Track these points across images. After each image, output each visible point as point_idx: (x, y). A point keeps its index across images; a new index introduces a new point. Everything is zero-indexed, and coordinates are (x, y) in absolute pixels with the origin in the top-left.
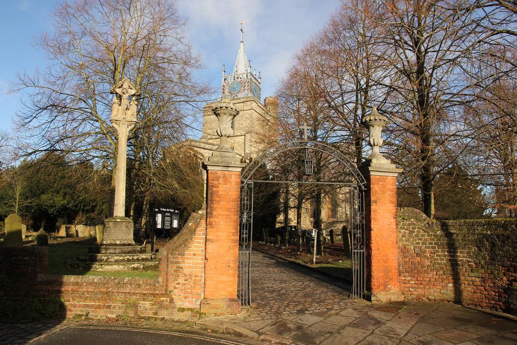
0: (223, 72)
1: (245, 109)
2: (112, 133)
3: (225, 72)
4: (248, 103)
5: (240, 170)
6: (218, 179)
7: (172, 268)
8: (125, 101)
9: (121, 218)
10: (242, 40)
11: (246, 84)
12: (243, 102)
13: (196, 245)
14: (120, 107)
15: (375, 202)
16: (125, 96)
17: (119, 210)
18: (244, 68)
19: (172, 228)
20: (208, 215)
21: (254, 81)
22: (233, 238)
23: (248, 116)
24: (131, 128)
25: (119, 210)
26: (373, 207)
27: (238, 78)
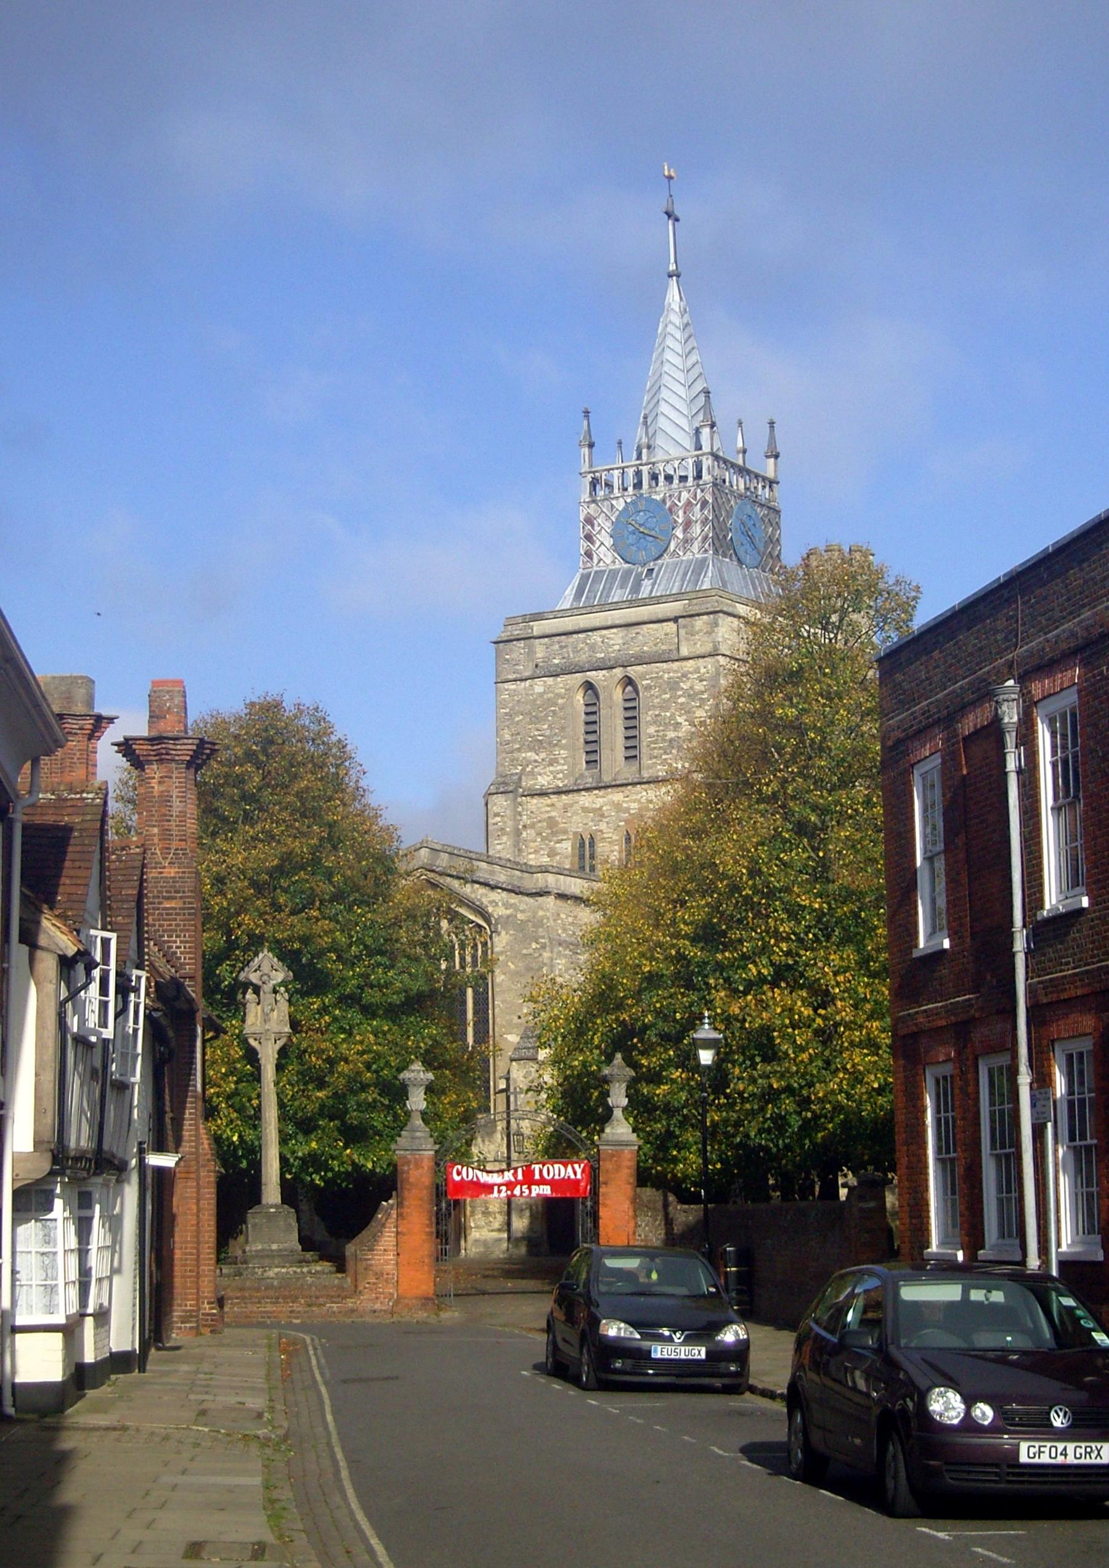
0: (586, 450)
1: (685, 651)
2: (252, 1056)
3: (591, 446)
4: (700, 623)
5: (432, 1153)
6: (408, 1163)
7: (361, 1267)
8: (267, 996)
9: (275, 1206)
10: (672, 267)
11: (697, 513)
12: (675, 620)
13: (388, 1239)
14: (259, 1007)
15: (606, 1183)
16: (267, 988)
17: (272, 1193)
18: (684, 423)
19: (668, 1149)
20: (400, 1205)
21: (740, 484)
22: (427, 1230)
23: (699, 687)
24: (280, 1043)
25: (272, 1193)
26: (602, 1190)
27: (654, 477)
